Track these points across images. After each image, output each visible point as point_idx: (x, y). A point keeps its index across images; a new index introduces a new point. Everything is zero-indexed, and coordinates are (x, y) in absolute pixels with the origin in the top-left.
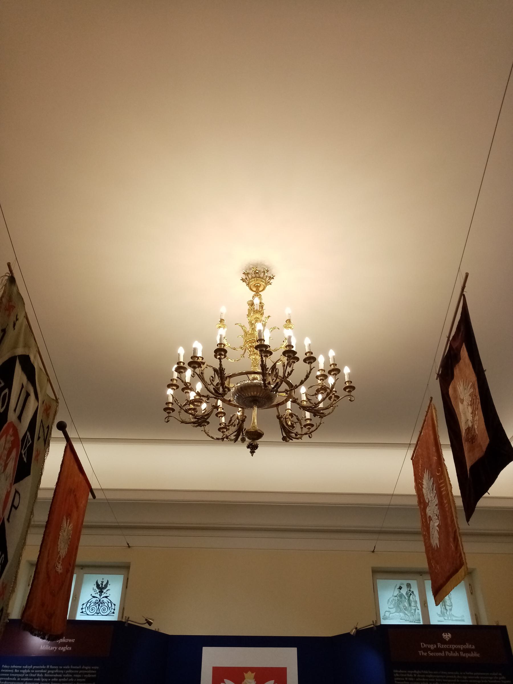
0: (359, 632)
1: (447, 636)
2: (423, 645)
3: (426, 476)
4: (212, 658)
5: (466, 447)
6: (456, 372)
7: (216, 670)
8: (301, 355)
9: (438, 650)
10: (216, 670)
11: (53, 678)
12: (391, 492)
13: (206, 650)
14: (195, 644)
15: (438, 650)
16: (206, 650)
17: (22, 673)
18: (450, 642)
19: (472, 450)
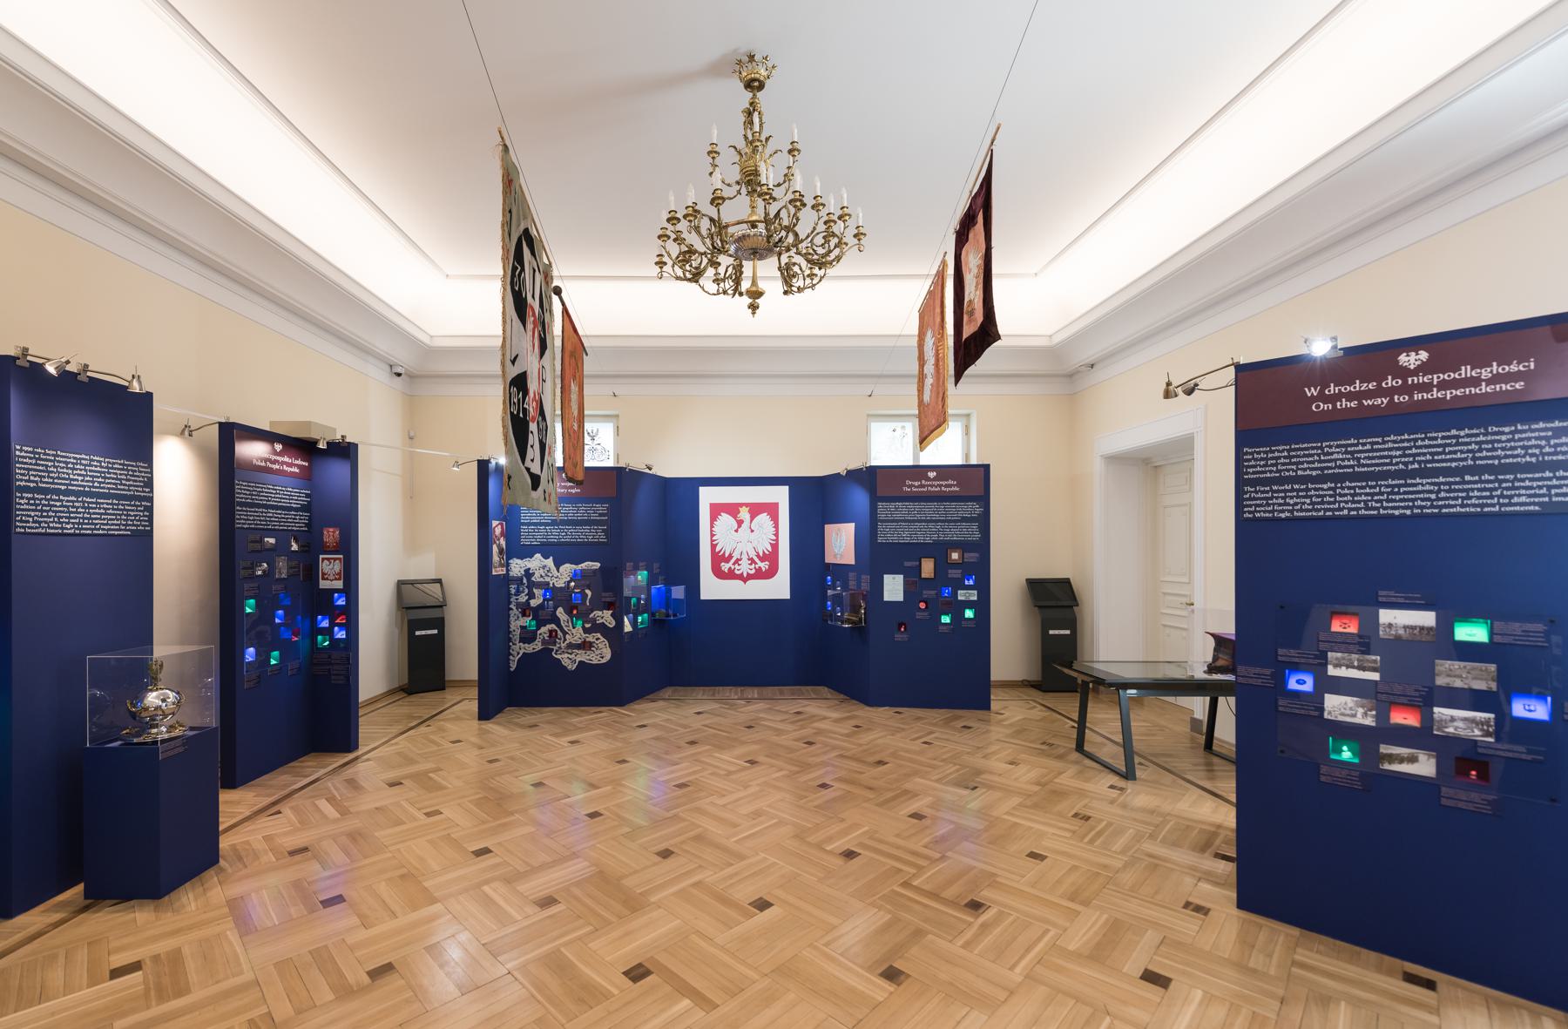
0: (849, 472)
1: (932, 475)
2: (908, 482)
3: (929, 334)
4: (707, 496)
5: (965, 318)
6: (971, 236)
7: (713, 506)
8: (809, 201)
9: (922, 486)
10: (713, 506)
11: (1508, 441)
12: (897, 332)
13: (702, 489)
14: (691, 486)
15: (922, 486)
16: (702, 489)
17: (1523, 447)
18: (935, 479)
19: (970, 321)
